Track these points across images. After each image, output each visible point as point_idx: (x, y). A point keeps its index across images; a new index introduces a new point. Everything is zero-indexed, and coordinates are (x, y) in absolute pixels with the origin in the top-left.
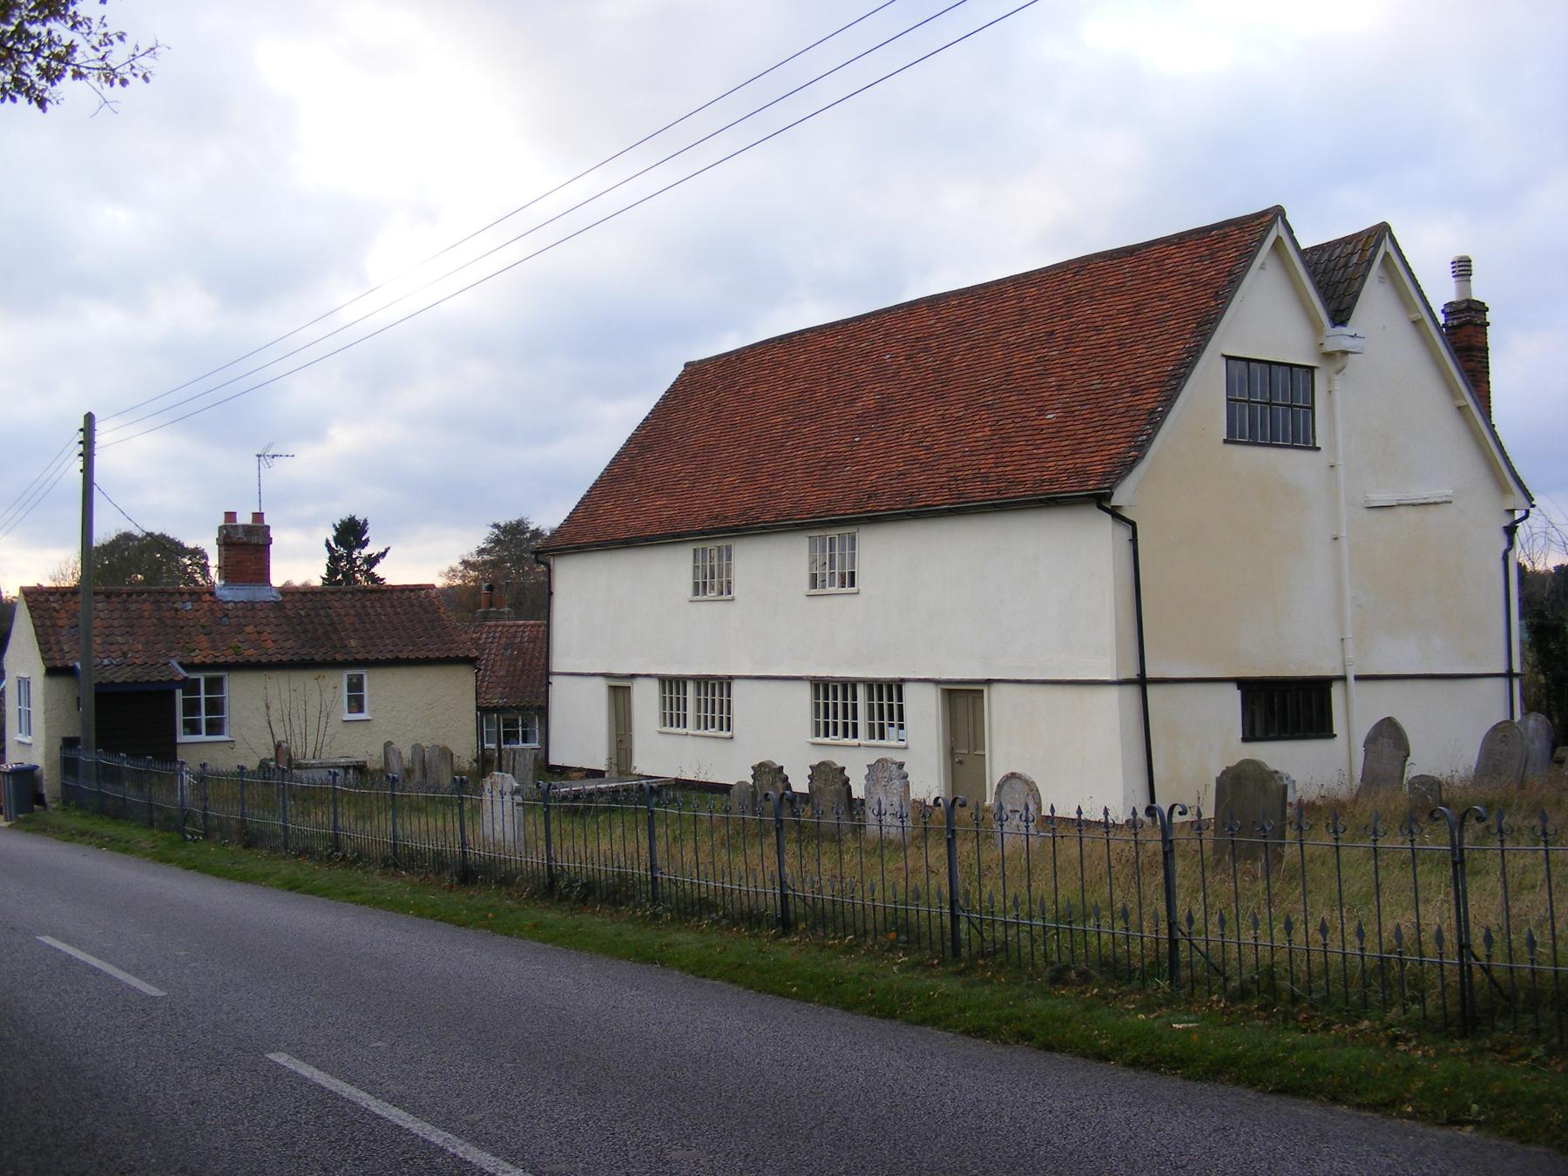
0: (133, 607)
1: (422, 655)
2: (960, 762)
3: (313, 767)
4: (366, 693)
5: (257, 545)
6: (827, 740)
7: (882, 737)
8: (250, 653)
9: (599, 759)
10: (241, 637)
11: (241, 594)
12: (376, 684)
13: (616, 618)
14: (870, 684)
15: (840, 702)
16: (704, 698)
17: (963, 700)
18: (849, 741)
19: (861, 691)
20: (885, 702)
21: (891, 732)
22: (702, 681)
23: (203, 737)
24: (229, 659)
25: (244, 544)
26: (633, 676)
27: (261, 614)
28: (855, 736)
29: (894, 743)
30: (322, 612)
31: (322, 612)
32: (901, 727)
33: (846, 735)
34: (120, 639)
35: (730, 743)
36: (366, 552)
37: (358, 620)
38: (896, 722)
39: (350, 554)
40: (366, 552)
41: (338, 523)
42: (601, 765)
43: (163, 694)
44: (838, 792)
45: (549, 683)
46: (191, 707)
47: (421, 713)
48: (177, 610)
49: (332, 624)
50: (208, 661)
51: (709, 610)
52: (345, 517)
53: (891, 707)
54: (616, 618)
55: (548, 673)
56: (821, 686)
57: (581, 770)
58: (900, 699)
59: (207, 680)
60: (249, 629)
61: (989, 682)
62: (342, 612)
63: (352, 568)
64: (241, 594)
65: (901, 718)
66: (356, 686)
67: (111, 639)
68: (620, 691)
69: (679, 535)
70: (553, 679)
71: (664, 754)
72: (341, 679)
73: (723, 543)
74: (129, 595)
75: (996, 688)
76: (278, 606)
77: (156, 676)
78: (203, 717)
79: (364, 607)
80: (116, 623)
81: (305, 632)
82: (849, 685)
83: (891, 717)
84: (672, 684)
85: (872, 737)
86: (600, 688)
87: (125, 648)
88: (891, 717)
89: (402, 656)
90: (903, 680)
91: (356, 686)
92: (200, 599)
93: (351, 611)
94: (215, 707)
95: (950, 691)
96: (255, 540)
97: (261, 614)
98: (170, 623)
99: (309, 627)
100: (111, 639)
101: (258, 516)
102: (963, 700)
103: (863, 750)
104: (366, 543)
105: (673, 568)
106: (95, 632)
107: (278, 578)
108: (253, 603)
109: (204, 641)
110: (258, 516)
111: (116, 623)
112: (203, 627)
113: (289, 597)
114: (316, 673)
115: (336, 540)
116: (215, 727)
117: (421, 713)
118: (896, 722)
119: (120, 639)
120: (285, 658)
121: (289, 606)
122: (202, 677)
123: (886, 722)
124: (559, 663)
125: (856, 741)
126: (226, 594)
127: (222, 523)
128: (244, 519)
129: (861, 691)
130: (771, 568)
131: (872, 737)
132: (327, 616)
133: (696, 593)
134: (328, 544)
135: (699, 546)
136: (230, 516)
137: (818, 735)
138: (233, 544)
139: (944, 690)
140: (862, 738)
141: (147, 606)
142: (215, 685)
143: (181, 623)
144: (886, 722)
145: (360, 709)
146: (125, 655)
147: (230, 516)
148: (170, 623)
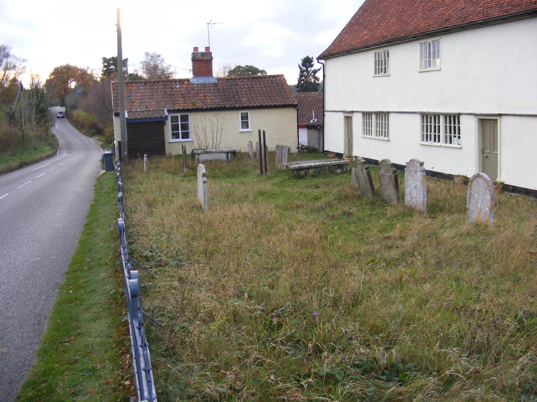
0: (155, 87)
1: (272, 104)
2: (487, 157)
3: (212, 152)
4: (249, 120)
5: (207, 60)
6: (427, 143)
7: (451, 143)
8: (199, 105)
9: (340, 149)
10: (197, 98)
11: (201, 80)
12: (254, 116)
13: (349, 85)
14: (446, 116)
15: (433, 124)
16: (378, 120)
17: (488, 123)
18: (436, 144)
19: (442, 119)
20: (452, 125)
21: (455, 140)
22: (447, 116)
23: (180, 140)
24: (190, 108)
25: (201, 60)
26: (352, 112)
27: (208, 89)
28: (439, 141)
29: (456, 146)
30: (234, 87)
31: (234, 87)
32: (459, 137)
33: (435, 141)
34: (147, 101)
35: (388, 142)
36: (313, 68)
37: (249, 90)
38: (457, 135)
39: (307, 70)
40: (313, 68)
41: (303, 59)
42: (341, 151)
43: (162, 122)
44: (391, 177)
45: (324, 115)
46: (175, 128)
47: (280, 129)
48: (173, 88)
49: (237, 91)
50: (180, 108)
51: (382, 80)
52: (305, 57)
53: (455, 127)
54: (349, 85)
55: (324, 111)
56: (425, 116)
57: (333, 153)
58: (459, 124)
59: (181, 116)
60: (202, 95)
61: (500, 115)
62: (242, 87)
63: (308, 74)
64: (201, 80)
65: (459, 134)
66: (245, 118)
67: (143, 101)
68: (348, 119)
69: (367, 47)
70: (326, 114)
71: (366, 148)
72: (237, 116)
73: (385, 49)
74: (154, 83)
75: (504, 118)
76: (215, 85)
77: (156, 115)
78: (180, 131)
79: (252, 84)
80: (146, 94)
81: (225, 95)
82: (436, 116)
83: (455, 133)
84: (367, 115)
85: (446, 142)
86: (341, 116)
87: (148, 104)
88: (455, 133)
89: (264, 104)
90: (460, 114)
91: (245, 118)
92: (183, 83)
93: (246, 86)
94: (185, 127)
95: (482, 120)
96: (205, 58)
97: (208, 89)
98: (168, 93)
99: (227, 94)
100: (143, 101)
101: (207, 49)
102: (488, 123)
103: (442, 149)
104: (312, 66)
105: (366, 61)
106: (125, 95)
107: (214, 75)
108: (205, 84)
109: (181, 100)
110: (207, 49)
111: (146, 94)
112: (182, 94)
113: (221, 81)
114: (215, 113)
115: (303, 65)
116: (186, 136)
117: (280, 129)
118: (457, 135)
119: (147, 101)
120: (213, 107)
121: (220, 85)
122: (179, 115)
123: (452, 135)
124: (327, 107)
125: (439, 144)
126: (195, 81)
127: (193, 52)
128: (202, 50)
129: (442, 119)
130: (405, 58)
131: (446, 142)
132: (235, 89)
133: (376, 73)
134: (299, 66)
135: (377, 51)
136: (196, 49)
137: (423, 140)
138: (196, 60)
139: (479, 119)
140: (442, 143)
141: (161, 87)
142: (185, 119)
143: (173, 93)
144: (452, 135)
145: (247, 127)
146: (147, 107)
147: (196, 49)
148: (168, 93)
